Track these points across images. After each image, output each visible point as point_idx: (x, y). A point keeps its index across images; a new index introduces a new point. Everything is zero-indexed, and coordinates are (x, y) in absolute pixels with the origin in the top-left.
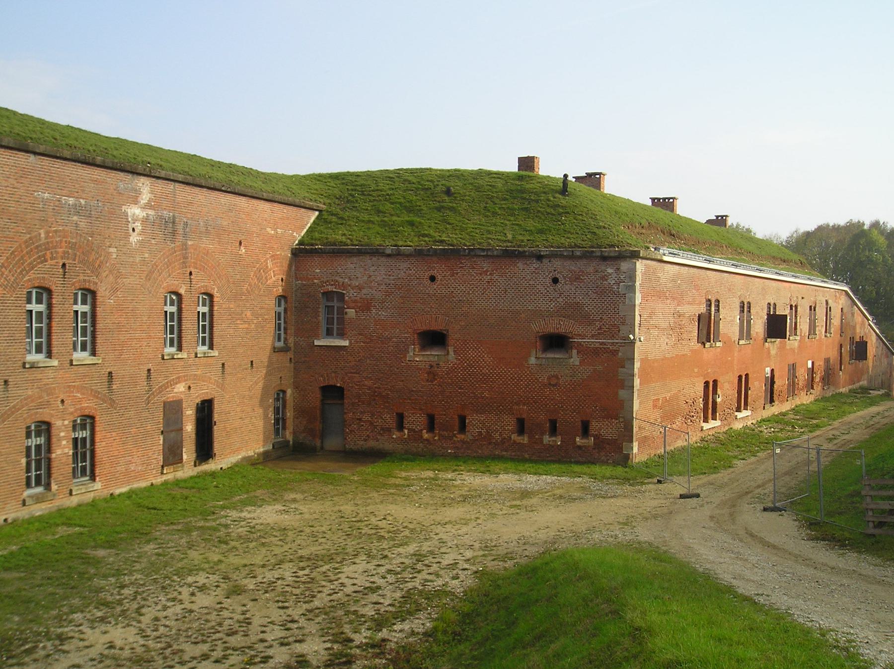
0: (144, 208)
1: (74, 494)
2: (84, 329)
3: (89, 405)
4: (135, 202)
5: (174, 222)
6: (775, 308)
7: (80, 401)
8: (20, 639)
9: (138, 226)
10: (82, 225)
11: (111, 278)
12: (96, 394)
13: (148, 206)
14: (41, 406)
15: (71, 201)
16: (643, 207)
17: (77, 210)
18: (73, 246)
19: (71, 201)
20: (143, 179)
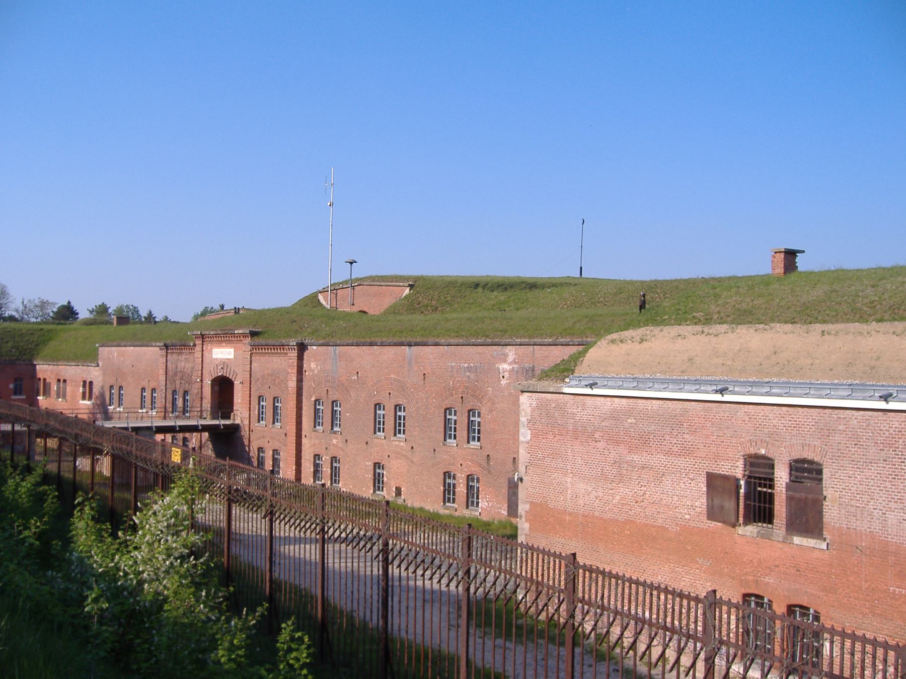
0: (510, 364)
1: (459, 510)
2: (379, 424)
3: (475, 470)
4: (505, 361)
5: (533, 370)
6: (335, 474)
7: (470, 466)
8: (588, 612)
9: (507, 375)
10: (472, 376)
11: (489, 404)
12: (480, 465)
13: (514, 362)
14: (450, 464)
15: (466, 365)
16: (765, 280)
17: (469, 369)
18: (467, 388)
19: (466, 365)
20: (509, 347)
